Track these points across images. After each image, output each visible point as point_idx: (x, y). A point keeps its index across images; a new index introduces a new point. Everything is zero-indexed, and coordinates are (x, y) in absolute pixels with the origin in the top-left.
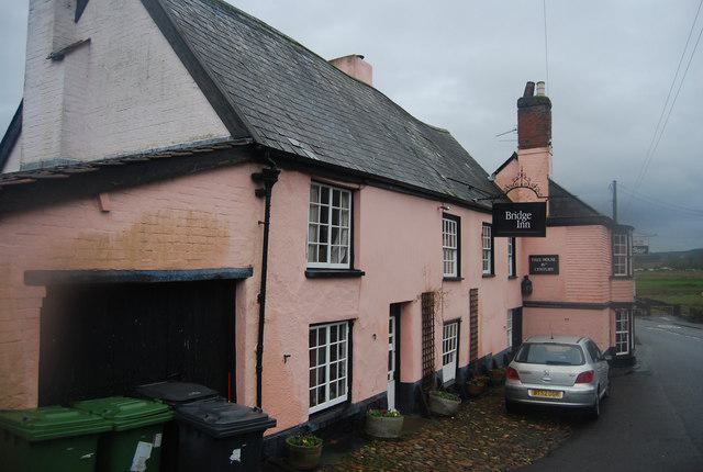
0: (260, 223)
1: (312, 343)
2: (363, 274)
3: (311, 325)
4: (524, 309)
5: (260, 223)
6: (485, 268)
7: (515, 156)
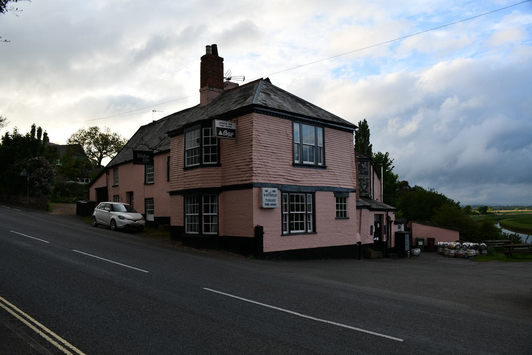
2: (349, 218)
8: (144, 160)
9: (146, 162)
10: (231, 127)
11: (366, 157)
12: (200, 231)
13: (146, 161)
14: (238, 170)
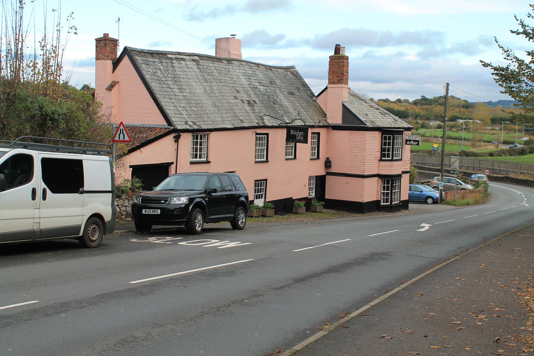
0: (176, 149)
2: (210, 162)
4: (327, 177)
5: (176, 149)
6: (313, 154)
7: (326, 88)
8: (298, 138)
9: (299, 140)
10: (416, 139)
12: (393, 137)
13: (299, 138)
14: (404, 163)
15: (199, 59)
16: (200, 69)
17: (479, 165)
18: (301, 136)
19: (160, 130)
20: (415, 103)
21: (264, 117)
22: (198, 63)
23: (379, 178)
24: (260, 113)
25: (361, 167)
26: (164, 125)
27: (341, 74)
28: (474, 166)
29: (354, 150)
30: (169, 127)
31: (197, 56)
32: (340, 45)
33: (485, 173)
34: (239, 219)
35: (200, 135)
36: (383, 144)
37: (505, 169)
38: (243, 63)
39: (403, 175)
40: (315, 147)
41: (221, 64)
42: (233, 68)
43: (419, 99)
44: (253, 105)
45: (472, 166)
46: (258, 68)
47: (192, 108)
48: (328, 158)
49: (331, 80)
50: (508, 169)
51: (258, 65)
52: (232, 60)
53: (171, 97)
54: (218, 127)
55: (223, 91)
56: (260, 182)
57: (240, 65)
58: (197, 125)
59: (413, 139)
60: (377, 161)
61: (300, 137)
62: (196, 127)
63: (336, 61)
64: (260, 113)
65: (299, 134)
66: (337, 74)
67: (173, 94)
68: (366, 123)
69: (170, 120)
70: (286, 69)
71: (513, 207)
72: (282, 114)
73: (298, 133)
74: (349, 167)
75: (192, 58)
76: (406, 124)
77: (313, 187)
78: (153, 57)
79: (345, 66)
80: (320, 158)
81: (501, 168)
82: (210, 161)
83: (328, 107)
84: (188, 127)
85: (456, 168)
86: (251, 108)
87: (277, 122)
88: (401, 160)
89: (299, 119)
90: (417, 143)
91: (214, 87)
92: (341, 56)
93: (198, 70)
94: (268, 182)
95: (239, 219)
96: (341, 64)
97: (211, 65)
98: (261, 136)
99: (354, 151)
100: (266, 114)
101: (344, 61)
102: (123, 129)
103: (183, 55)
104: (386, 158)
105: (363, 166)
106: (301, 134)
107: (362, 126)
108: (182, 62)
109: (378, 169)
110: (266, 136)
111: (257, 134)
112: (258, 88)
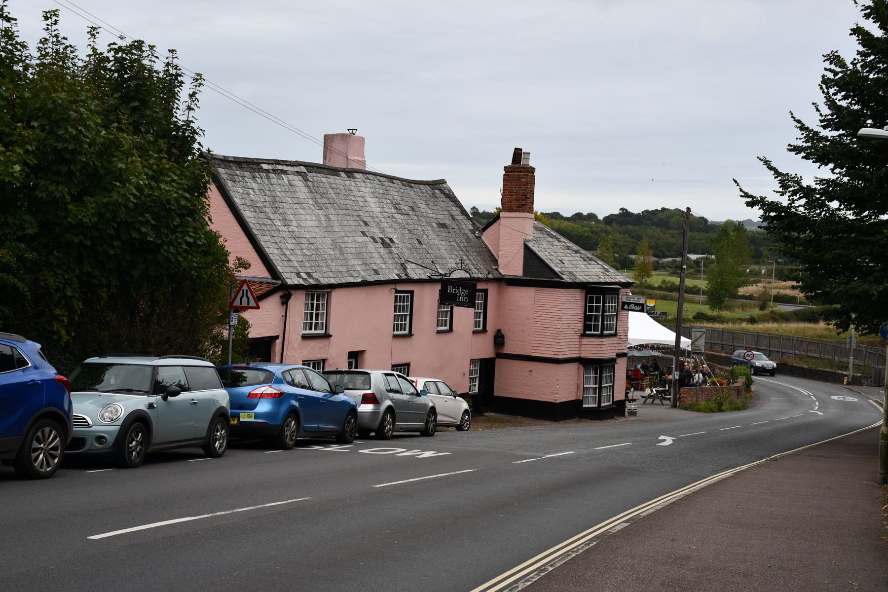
1: (396, 302)
2: (331, 336)
3: (303, 361)
4: (497, 360)
5: (283, 316)
6: (477, 324)
8: (459, 299)
9: (461, 301)
11: (838, 306)
13: (462, 299)
15: (306, 171)
16: (308, 187)
17: (733, 342)
18: (465, 296)
19: (261, 286)
20: (609, 219)
21: (407, 265)
22: (305, 178)
23: (580, 364)
24: (400, 258)
25: (554, 346)
26: (265, 278)
27: (522, 195)
28: (724, 343)
29: (541, 318)
30: (274, 281)
31: (304, 166)
32: (521, 150)
33: (746, 357)
34: (35, 445)
35: (318, 293)
36: (588, 309)
37: (778, 350)
38: (370, 177)
39: (619, 360)
40: (480, 313)
41: (338, 178)
42: (356, 184)
43: (616, 214)
44: (390, 245)
45: (720, 342)
46: (392, 185)
47: (304, 251)
48: (499, 331)
49: (507, 205)
50: (784, 350)
51: (391, 179)
52: (354, 172)
53: (273, 233)
54: (344, 282)
55: (345, 223)
56: (399, 368)
57: (365, 180)
58: (313, 278)
59: (633, 302)
60: (578, 337)
61: (464, 297)
62: (312, 281)
63: (514, 175)
64: (400, 258)
65: (462, 293)
66: (516, 195)
67: (274, 228)
68: (563, 276)
69: (276, 270)
70: (432, 185)
71: (796, 415)
72: (432, 260)
73: (459, 291)
74: (534, 345)
75: (296, 169)
76: (622, 277)
77: (476, 378)
78: (241, 168)
79: (530, 183)
80: (487, 329)
81: (773, 347)
82: (331, 334)
83: (500, 248)
84: (302, 282)
85: (700, 349)
86: (386, 251)
87: (425, 272)
88: (614, 335)
89: (461, 270)
90: (641, 308)
91: (331, 216)
92: (523, 168)
93: (306, 190)
94: (411, 368)
95: (35, 445)
96: (523, 180)
97: (324, 180)
98: (402, 295)
99: (542, 321)
100: (409, 260)
101: (527, 175)
102: (247, 290)
103: (283, 165)
104: (592, 332)
105: (555, 344)
106: (464, 293)
107: (556, 280)
108: (283, 175)
109: (578, 349)
110: (409, 295)
111: (397, 291)
112: (394, 218)
